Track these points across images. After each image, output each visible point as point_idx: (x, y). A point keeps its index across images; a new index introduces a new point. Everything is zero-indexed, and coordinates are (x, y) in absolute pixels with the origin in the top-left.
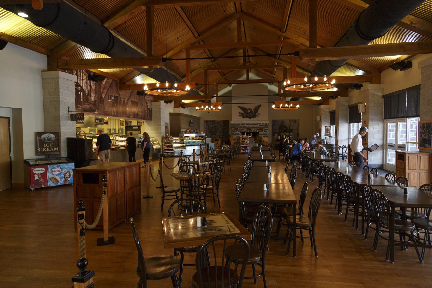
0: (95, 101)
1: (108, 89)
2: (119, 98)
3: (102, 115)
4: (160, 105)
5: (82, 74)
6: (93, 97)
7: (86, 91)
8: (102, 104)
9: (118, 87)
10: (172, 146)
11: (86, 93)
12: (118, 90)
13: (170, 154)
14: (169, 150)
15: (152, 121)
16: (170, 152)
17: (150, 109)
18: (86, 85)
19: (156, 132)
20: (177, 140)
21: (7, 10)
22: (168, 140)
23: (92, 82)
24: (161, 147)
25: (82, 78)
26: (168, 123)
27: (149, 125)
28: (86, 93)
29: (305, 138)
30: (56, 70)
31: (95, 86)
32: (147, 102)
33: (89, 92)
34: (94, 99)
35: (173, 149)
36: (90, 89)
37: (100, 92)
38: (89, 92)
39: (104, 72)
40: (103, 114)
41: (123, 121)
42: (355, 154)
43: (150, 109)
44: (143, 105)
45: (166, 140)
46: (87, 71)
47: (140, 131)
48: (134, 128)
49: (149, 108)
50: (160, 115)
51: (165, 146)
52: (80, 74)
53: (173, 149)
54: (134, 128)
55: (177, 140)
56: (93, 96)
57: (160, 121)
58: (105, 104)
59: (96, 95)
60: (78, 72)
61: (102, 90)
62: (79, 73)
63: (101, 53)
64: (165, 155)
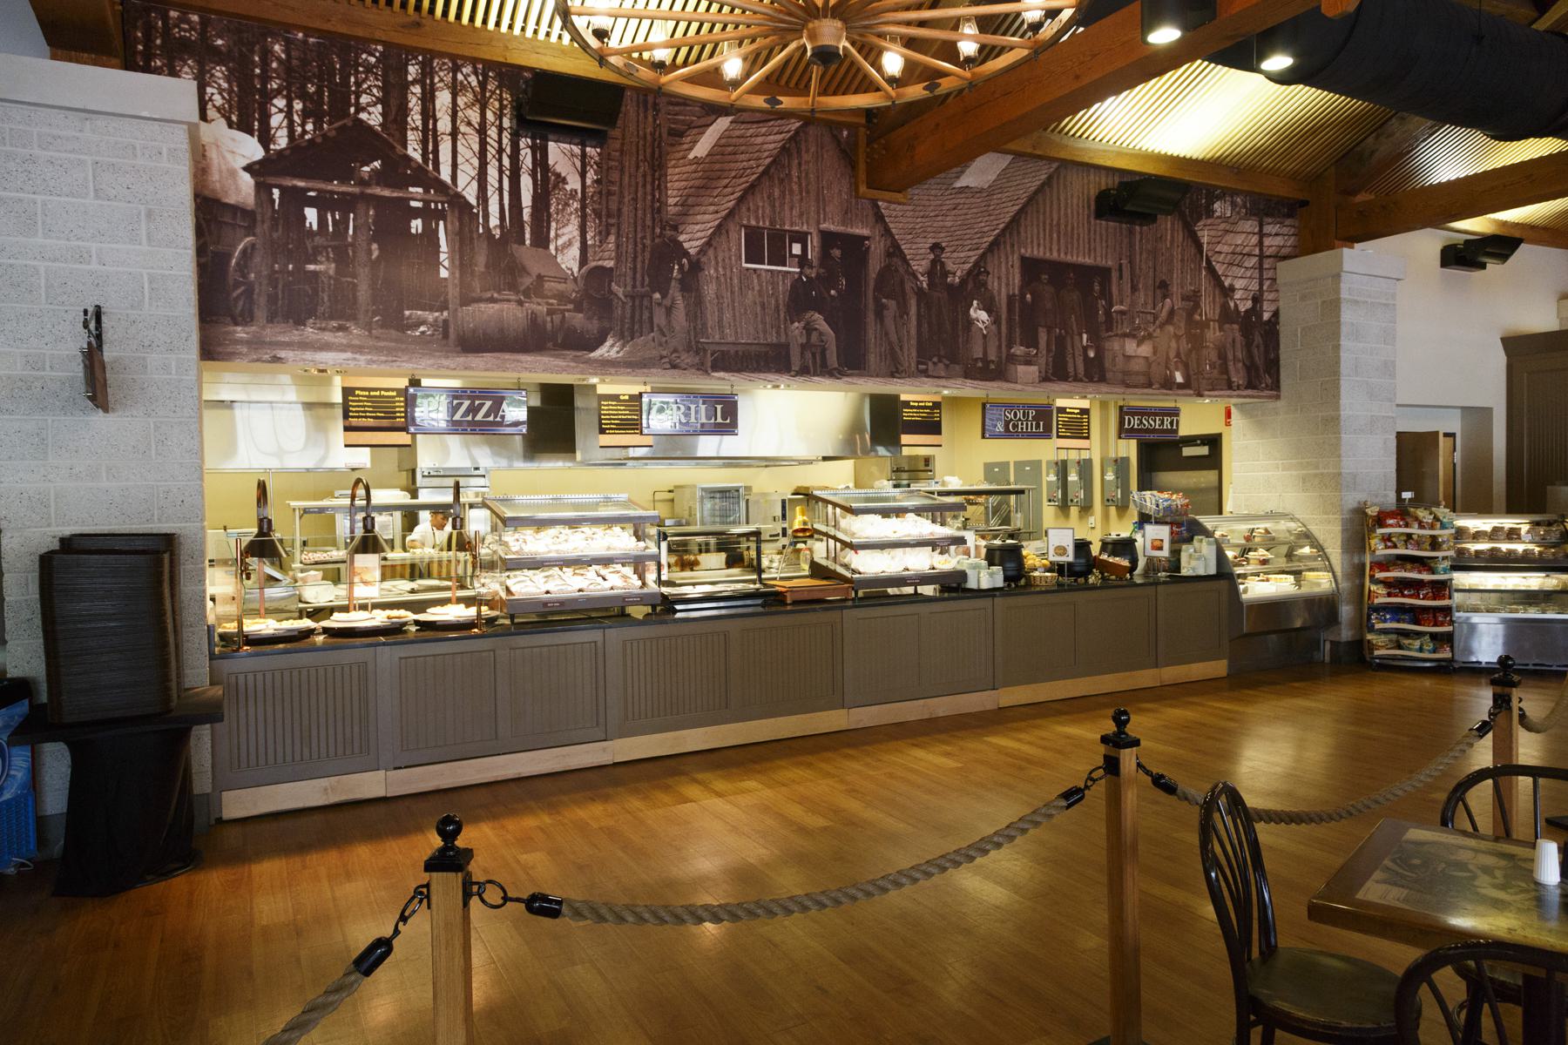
0: (597, 277)
1: (752, 188)
2: (877, 249)
3: (674, 367)
4: (1337, 277)
5: (443, 99)
6: (575, 251)
7: (494, 208)
8: (675, 291)
9: (862, 167)
10: (1441, 588)
11: (494, 221)
12: (863, 189)
13: (1417, 644)
14: (1416, 614)
15: (1278, 397)
16: (1419, 634)
17: (1255, 310)
18: (492, 172)
19: (1304, 479)
20: (1513, 535)
21: (1467, 127)
22: (1409, 536)
23: (559, 154)
24: (1344, 585)
25: (444, 125)
26: (1485, 413)
27: (1260, 425)
28: (494, 221)
29: (1173, 798)
30: (1333, 248)
31: (591, 176)
32: (1220, 269)
33: (526, 214)
34: (583, 261)
35: (1447, 611)
36: (541, 200)
37: (658, 208)
38: (526, 214)
39: (1202, 161)
40: (687, 358)
41: (1085, 412)
42: (225, 223)
43: (1255, 310)
44: (1175, 289)
45: (1387, 539)
46: (500, 77)
47: (1216, 472)
48: (1188, 451)
49: (1245, 306)
50: (1337, 347)
51: (1374, 580)
52: (428, 99)
53: (1447, 611)
54: (1188, 451)
55: (1513, 535)
56: (569, 244)
57: (1336, 396)
58: (710, 291)
59: (603, 235)
60: (405, 86)
61: (671, 201)
62: (417, 89)
63: (1506, 141)
64: (1372, 647)
